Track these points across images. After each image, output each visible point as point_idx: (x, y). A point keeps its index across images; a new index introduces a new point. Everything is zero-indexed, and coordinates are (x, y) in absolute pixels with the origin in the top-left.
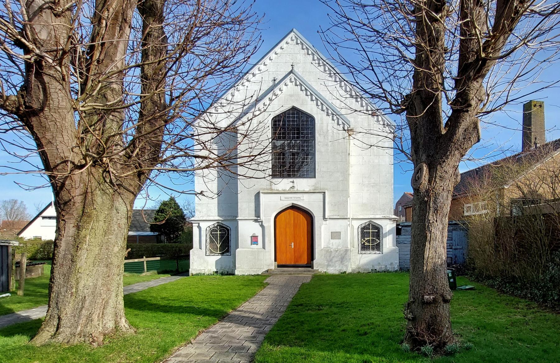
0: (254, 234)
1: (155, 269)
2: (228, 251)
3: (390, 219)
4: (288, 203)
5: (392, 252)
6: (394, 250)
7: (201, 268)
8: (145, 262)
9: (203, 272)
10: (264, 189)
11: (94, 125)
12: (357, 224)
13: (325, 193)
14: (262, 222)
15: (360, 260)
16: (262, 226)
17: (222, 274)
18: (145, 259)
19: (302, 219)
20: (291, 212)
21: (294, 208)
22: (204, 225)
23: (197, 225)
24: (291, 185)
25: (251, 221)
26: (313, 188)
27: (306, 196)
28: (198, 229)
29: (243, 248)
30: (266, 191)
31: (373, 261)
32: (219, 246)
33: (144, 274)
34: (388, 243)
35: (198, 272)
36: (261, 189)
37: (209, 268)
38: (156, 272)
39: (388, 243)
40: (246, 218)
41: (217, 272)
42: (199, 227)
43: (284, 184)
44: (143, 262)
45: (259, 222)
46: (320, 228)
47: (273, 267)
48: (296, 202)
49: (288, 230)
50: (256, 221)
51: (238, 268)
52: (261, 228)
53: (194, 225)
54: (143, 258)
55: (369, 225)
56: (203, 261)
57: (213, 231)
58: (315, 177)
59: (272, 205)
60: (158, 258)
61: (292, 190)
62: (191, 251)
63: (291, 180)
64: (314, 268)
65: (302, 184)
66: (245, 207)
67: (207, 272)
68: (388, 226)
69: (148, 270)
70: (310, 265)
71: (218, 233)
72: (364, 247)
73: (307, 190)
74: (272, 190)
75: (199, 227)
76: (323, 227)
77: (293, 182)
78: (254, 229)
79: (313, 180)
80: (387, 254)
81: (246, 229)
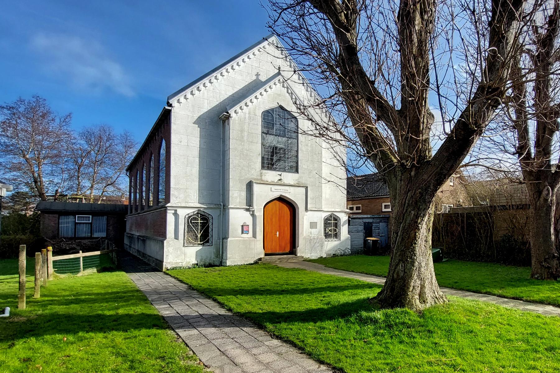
0: (245, 223)
1: (95, 266)
2: (208, 242)
3: (345, 212)
4: (276, 195)
5: (347, 239)
6: (348, 238)
7: (178, 261)
8: (81, 259)
9: (180, 265)
10: (257, 180)
11: (491, 139)
12: (325, 215)
13: (307, 187)
14: (253, 211)
15: (330, 246)
16: (253, 215)
17: (206, 266)
18: (81, 255)
19: (286, 210)
20: (277, 202)
21: (281, 199)
22: (183, 213)
23: (173, 212)
24: (279, 177)
25: (243, 211)
26: (297, 182)
27: (292, 188)
28: (173, 217)
29: (234, 237)
30: (258, 182)
31: (337, 246)
32: (199, 236)
33: (80, 275)
34: (344, 231)
35: (174, 266)
36: (255, 179)
37: (188, 260)
38: (95, 270)
39: (344, 231)
40: (238, 207)
41: (197, 264)
42: (176, 214)
43: (271, 176)
44: (79, 258)
45: (250, 211)
46: (303, 219)
47: (262, 256)
48: (284, 194)
49: (274, 220)
50: (248, 210)
51: (229, 258)
52: (251, 218)
53: (168, 211)
54: (78, 253)
55: (331, 216)
56: (179, 252)
57: (191, 220)
58: (297, 171)
59: (263, 195)
60: (98, 253)
61: (280, 182)
62: (165, 242)
63: (280, 173)
64: (298, 255)
65: (289, 177)
66: (236, 195)
67: (184, 265)
68: (344, 218)
69: (85, 268)
70: (293, 251)
71: (199, 221)
72: (327, 235)
73: (292, 183)
74: (262, 181)
75: (176, 214)
76: (305, 217)
77: (280, 175)
78: (246, 218)
79: (296, 175)
80: (343, 242)
81: (238, 217)
